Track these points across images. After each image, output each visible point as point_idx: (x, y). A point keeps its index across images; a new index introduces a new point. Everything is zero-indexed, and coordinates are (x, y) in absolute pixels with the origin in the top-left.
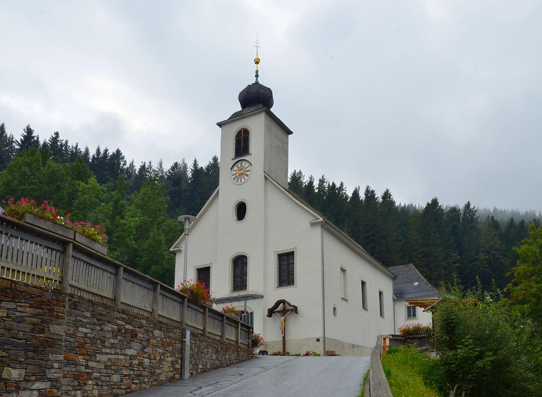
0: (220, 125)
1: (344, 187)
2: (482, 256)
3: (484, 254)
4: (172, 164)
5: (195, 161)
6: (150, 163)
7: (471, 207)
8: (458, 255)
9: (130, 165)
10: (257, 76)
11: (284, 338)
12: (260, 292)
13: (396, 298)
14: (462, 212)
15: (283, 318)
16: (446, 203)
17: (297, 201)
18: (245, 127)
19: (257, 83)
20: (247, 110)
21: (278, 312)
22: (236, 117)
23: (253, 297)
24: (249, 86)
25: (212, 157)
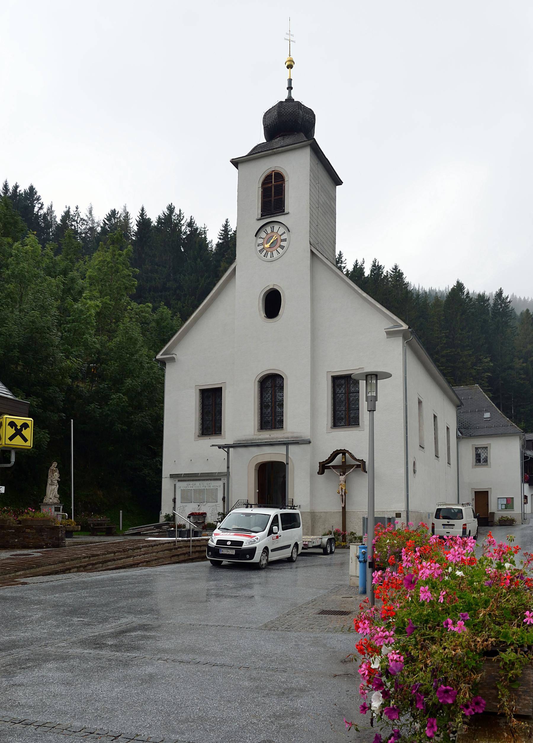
0: (236, 163)
1: (343, 259)
2: (518, 363)
3: (521, 361)
4: (108, 211)
5: (143, 210)
6: (77, 208)
7: (504, 295)
8: (491, 361)
9: (48, 209)
10: (290, 88)
11: (344, 508)
12: (305, 432)
13: (460, 434)
14: (491, 302)
15: (342, 478)
16: (474, 287)
17: (365, 295)
18: (277, 169)
19: (290, 99)
20: (278, 142)
21: (334, 467)
22: (258, 153)
23: (297, 442)
24: (281, 102)
25: (167, 205)
